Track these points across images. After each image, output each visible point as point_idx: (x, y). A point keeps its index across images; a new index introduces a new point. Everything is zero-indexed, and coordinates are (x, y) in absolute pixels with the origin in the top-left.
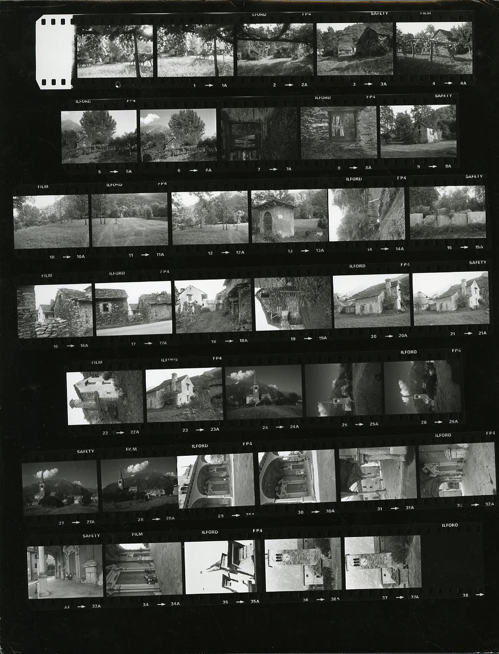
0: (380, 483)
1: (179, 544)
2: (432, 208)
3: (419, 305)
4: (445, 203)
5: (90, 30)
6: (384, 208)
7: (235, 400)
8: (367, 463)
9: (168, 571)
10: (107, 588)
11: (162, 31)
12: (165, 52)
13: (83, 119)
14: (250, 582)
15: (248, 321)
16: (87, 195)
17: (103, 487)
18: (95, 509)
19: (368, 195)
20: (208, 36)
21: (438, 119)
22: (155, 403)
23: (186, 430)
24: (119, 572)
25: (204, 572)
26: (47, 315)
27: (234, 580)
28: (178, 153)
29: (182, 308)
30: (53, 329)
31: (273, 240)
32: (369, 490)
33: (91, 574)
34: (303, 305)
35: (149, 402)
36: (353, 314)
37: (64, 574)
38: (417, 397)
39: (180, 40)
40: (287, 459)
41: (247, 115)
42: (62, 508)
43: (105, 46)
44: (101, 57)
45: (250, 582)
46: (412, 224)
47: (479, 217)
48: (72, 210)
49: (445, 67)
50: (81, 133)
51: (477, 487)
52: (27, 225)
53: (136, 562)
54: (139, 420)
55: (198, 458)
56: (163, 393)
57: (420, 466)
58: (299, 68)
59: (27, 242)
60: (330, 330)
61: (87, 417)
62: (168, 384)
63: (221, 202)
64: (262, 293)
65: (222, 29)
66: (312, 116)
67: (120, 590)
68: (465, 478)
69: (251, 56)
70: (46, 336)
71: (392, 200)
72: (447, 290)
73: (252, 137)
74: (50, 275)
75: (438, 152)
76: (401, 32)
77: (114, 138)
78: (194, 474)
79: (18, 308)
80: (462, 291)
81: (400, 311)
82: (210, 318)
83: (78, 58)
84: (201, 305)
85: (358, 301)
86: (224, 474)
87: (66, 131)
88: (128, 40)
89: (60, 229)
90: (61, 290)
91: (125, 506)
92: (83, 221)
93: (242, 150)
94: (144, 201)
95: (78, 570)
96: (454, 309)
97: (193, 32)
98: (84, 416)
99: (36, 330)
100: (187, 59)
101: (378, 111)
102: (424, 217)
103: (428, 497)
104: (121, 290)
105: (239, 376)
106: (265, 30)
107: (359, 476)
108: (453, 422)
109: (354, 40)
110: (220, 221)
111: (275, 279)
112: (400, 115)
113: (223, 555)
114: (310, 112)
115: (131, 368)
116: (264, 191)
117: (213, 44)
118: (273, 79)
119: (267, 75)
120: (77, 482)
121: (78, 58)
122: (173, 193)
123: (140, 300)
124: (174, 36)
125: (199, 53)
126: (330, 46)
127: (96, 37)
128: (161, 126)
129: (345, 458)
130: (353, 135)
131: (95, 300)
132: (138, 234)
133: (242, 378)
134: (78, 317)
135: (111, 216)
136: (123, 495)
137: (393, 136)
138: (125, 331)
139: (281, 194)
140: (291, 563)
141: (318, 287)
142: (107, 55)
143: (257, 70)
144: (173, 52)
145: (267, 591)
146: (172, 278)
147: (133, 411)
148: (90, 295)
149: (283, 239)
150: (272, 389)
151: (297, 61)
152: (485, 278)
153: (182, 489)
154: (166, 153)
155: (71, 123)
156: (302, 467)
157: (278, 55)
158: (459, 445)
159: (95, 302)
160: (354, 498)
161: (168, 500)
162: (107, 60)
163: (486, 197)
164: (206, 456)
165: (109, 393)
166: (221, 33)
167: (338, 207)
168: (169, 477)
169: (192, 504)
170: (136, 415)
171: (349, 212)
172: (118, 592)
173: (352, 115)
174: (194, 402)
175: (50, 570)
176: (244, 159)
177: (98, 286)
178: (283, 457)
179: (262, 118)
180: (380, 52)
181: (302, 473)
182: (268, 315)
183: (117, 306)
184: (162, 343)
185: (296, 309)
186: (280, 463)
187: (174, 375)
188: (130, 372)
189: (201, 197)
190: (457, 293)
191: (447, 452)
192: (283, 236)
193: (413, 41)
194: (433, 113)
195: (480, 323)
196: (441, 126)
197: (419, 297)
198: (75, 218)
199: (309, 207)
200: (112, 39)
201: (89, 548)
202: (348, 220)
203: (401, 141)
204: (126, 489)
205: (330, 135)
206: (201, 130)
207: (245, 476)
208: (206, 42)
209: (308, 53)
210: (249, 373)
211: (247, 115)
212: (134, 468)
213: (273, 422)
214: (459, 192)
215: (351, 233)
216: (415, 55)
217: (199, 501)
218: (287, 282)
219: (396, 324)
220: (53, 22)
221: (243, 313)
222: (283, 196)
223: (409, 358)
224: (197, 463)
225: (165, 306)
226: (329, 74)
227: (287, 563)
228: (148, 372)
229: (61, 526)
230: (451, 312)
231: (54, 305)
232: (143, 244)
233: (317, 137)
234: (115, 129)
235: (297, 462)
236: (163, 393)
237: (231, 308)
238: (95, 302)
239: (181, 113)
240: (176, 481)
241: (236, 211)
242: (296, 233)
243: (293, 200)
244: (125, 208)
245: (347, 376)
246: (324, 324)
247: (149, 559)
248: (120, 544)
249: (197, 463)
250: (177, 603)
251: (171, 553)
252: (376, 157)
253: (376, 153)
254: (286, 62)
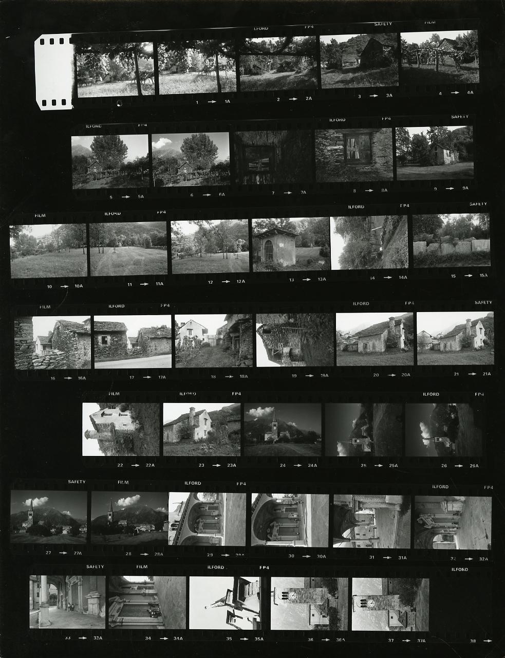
0: (374, 531)
1: (183, 578)
2: (435, 236)
3: (423, 345)
4: (449, 230)
5: (90, 48)
6: (387, 236)
7: (253, 436)
8: (362, 510)
9: (172, 605)
10: (110, 620)
11: (163, 47)
12: (166, 69)
13: (93, 144)
14: (255, 619)
15: (249, 357)
16: (85, 224)
17: (92, 519)
18: (83, 540)
19: (370, 222)
20: (209, 51)
21: (455, 141)
22: (171, 436)
23: (202, 465)
24: (122, 604)
25: (209, 607)
26: (44, 347)
27: (238, 617)
28: (101, 176)
29: (182, 342)
30: (51, 361)
31: (274, 269)
32: (362, 537)
33: (93, 605)
34: (305, 342)
35: (166, 435)
36: (356, 352)
37: (66, 604)
38: (438, 439)
39: (181, 56)
40: (280, 501)
41: (261, 138)
42: (49, 538)
43: (105, 64)
44: (101, 76)
45: (255, 619)
46: (415, 252)
47: (483, 245)
48: (69, 240)
49: (450, 77)
50: (92, 158)
51: (472, 542)
52: (24, 255)
53: (139, 594)
54: (155, 453)
55: (190, 496)
56: (180, 426)
57: (415, 516)
58: (303, 81)
59: (23, 271)
60: (331, 367)
61: (102, 448)
62: (185, 418)
63: (221, 231)
64: (264, 329)
65: (223, 44)
66: (326, 139)
67: (122, 622)
68: (461, 531)
69: (254, 71)
70: (42, 367)
71: (395, 228)
72: (451, 330)
73: (266, 160)
74: (49, 307)
75: (455, 174)
76: (406, 42)
77: (126, 163)
78: (185, 511)
79: (15, 339)
80: (467, 331)
81: (403, 350)
82: (210, 354)
83: (78, 78)
84: (202, 339)
85: (361, 339)
86: (216, 513)
87: (76, 157)
88: (128, 58)
89: (58, 259)
90: (60, 322)
91: (114, 539)
92: (82, 250)
93: (256, 173)
94: (144, 230)
95: (80, 601)
96: (458, 349)
97: (194, 48)
98: (99, 447)
99: (33, 361)
100: (189, 76)
101: (394, 132)
102: (428, 245)
103: (422, 548)
104: (120, 323)
105: (258, 412)
106: (267, 44)
107: (353, 523)
109: (358, 52)
110: (220, 250)
111: (277, 315)
112: (416, 136)
113: (229, 590)
114: (325, 135)
115: (148, 400)
116: (265, 219)
117: (215, 59)
118: (277, 94)
119: (271, 89)
120: (161, 509)
121: (78, 78)
122: (172, 222)
123: (140, 333)
124: (175, 52)
125: (201, 69)
126: (334, 58)
127: (96, 55)
128: (173, 150)
129: (340, 504)
130: (369, 157)
131: (94, 333)
132: (137, 263)
133: (261, 414)
134: (76, 349)
135: (109, 245)
136: (114, 528)
137: (409, 158)
138: (123, 364)
139: (282, 222)
140: (297, 601)
141: (321, 324)
142: (107, 73)
143: (261, 85)
144: (174, 68)
145: (272, 628)
146: (172, 312)
147: (149, 444)
148: (88, 327)
149: (284, 268)
150: (291, 427)
151: (300, 74)
152: (491, 318)
153: (172, 525)
154: (88, 177)
155: (81, 148)
156: (295, 510)
157: (280, 70)
158: (456, 497)
159: (93, 334)
160: (346, 545)
161: (158, 535)
162: (108, 78)
163: (490, 224)
164: (199, 493)
165: (126, 425)
166: (223, 49)
167: (340, 235)
168: (160, 513)
169: (182, 540)
170: (152, 448)
171: (351, 240)
172: (120, 624)
173: (368, 137)
174: (211, 438)
175: (52, 600)
176: (258, 183)
177: (97, 318)
178: (277, 500)
179: (276, 141)
180: (385, 62)
181: (295, 516)
182: (269, 351)
183: (116, 339)
184: (161, 377)
185: (298, 345)
186: (273, 505)
187: (192, 409)
188: (148, 404)
189: (201, 225)
190: (461, 333)
191: (444, 504)
192: (285, 265)
193: (418, 51)
194: (450, 134)
195: (484, 364)
196: (457, 147)
197: (423, 337)
198: (73, 247)
199: (310, 235)
200: (112, 57)
201: (92, 579)
202: (350, 249)
203: (417, 163)
204: (115, 522)
205: (346, 157)
206: (214, 154)
207: (237, 515)
208: (207, 58)
209: (311, 67)
210: (268, 410)
211: (261, 138)
212: (125, 502)
213: (291, 460)
214: (463, 220)
215: (353, 261)
216: (420, 66)
217: (189, 538)
218: (289, 319)
219: (399, 363)
220: (52, 42)
221: (243, 348)
222: (284, 224)
223: (431, 400)
224: (189, 500)
225: (165, 340)
226: (334, 86)
227: (293, 602)
228: (165, 405)
229: (48, 555)
230: (455, 352)
231: (52, 337)
232: (142, 274)
233: (332, 159)
234: (126, 154)
235: (291, 505)
236: (180, 426)
237: (232, 343)
238: (93, 334)
239: (193, 137)
240: (166, 517)
241: (237, 240)
242: (297, 262)
243: (294, 228)
244: (123, 237)
245: (367, 417)
246: (326, 362)
247: (152, 592)
248: (124, 577)
249: (189, 500)
251: (176, 587)
252: (392, 180)
253: (392, 175)
254: (290, 76)
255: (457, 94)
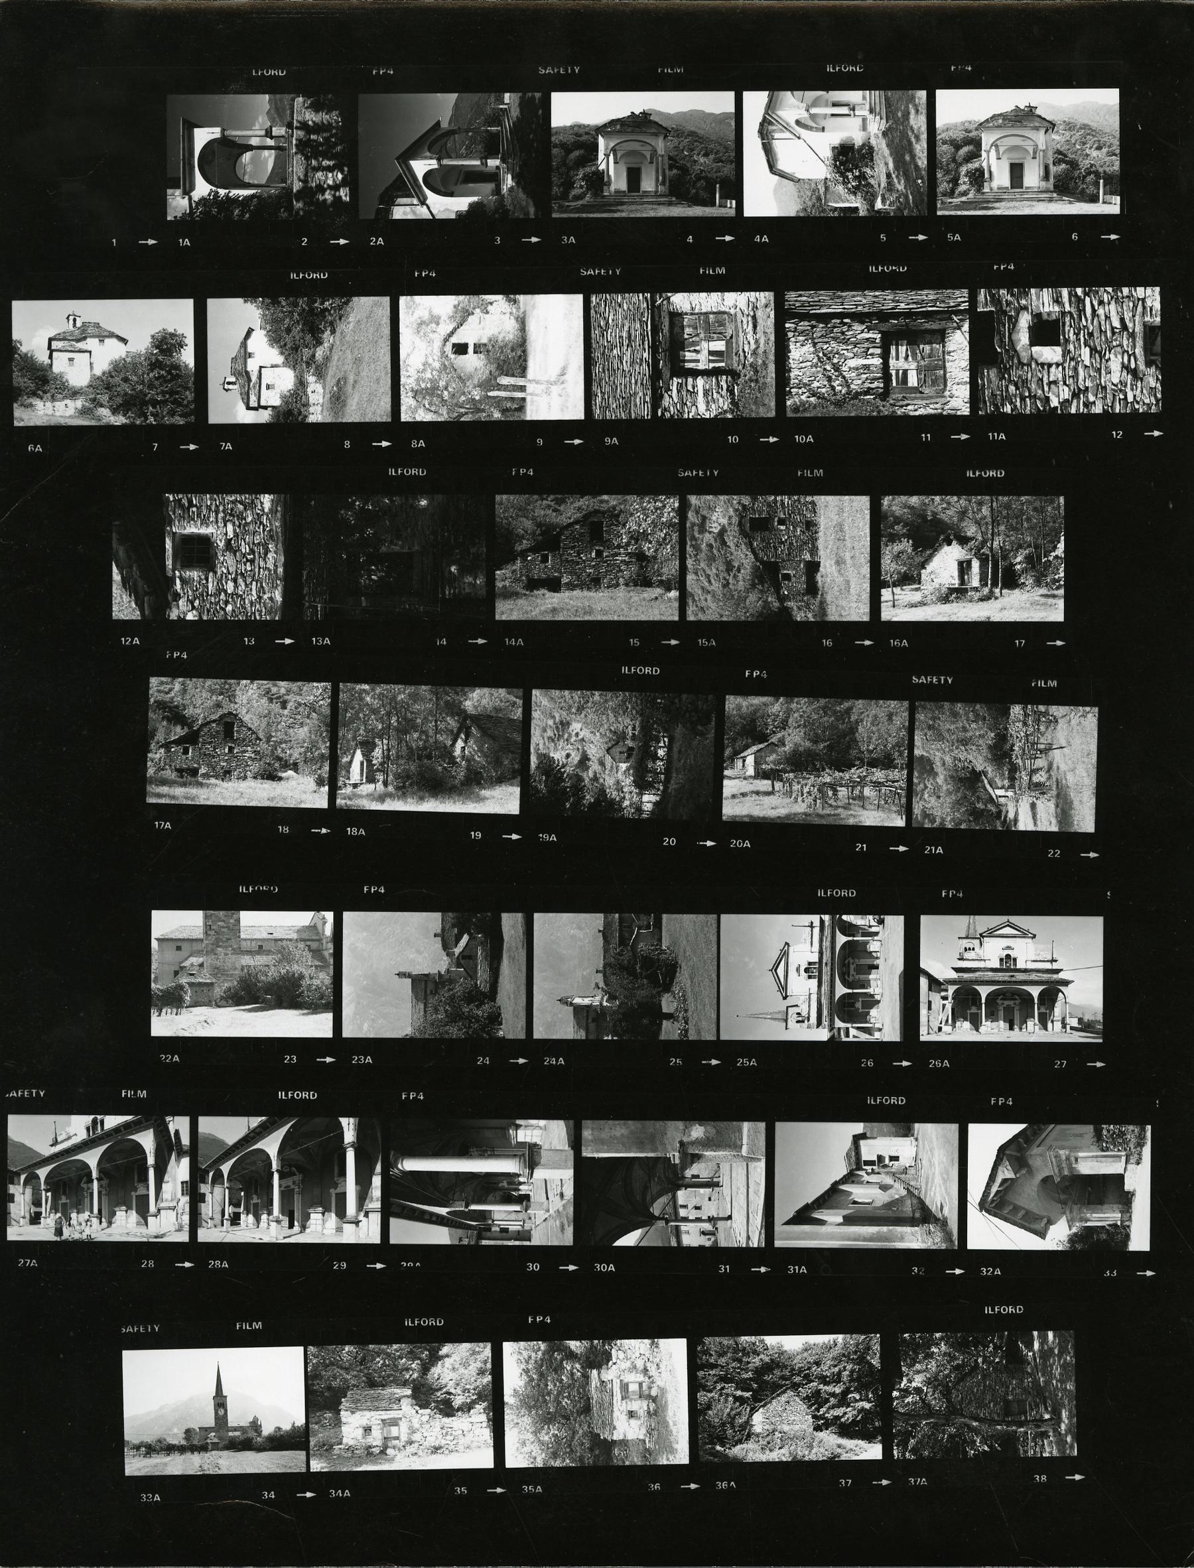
108: (938, 1064)
184: (160, 825)
250: (343, 1493)
255: (535, 243)
